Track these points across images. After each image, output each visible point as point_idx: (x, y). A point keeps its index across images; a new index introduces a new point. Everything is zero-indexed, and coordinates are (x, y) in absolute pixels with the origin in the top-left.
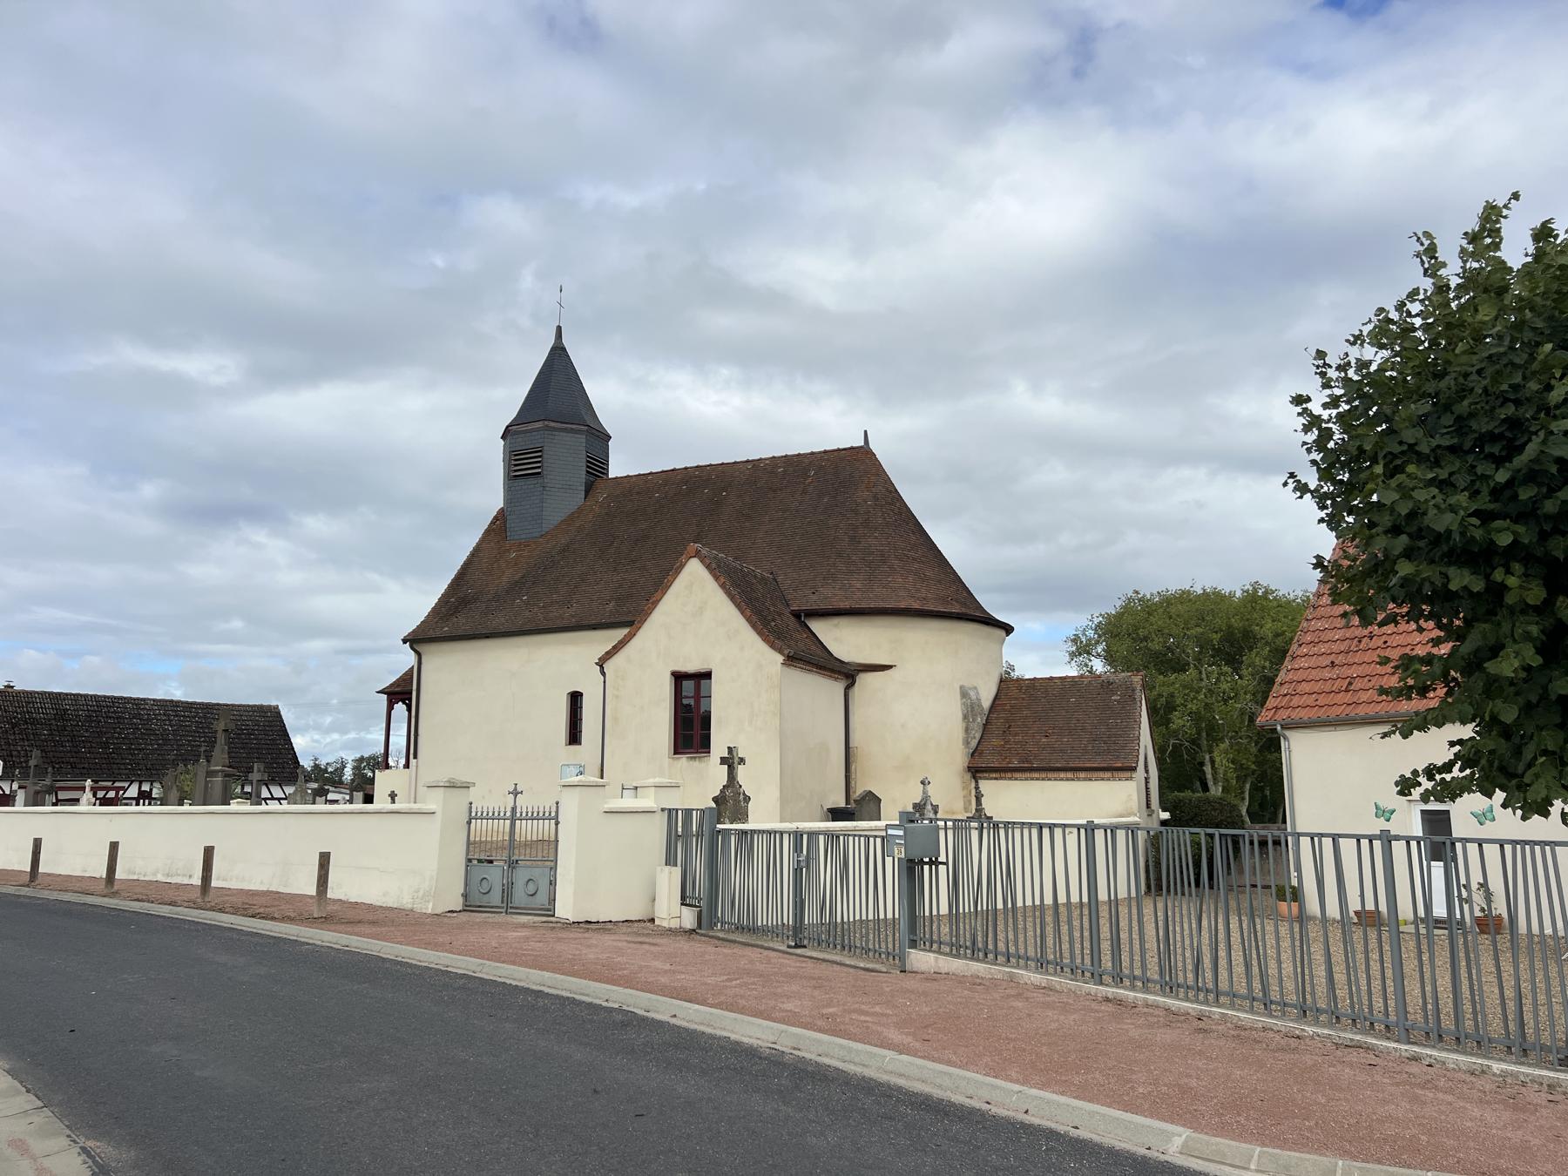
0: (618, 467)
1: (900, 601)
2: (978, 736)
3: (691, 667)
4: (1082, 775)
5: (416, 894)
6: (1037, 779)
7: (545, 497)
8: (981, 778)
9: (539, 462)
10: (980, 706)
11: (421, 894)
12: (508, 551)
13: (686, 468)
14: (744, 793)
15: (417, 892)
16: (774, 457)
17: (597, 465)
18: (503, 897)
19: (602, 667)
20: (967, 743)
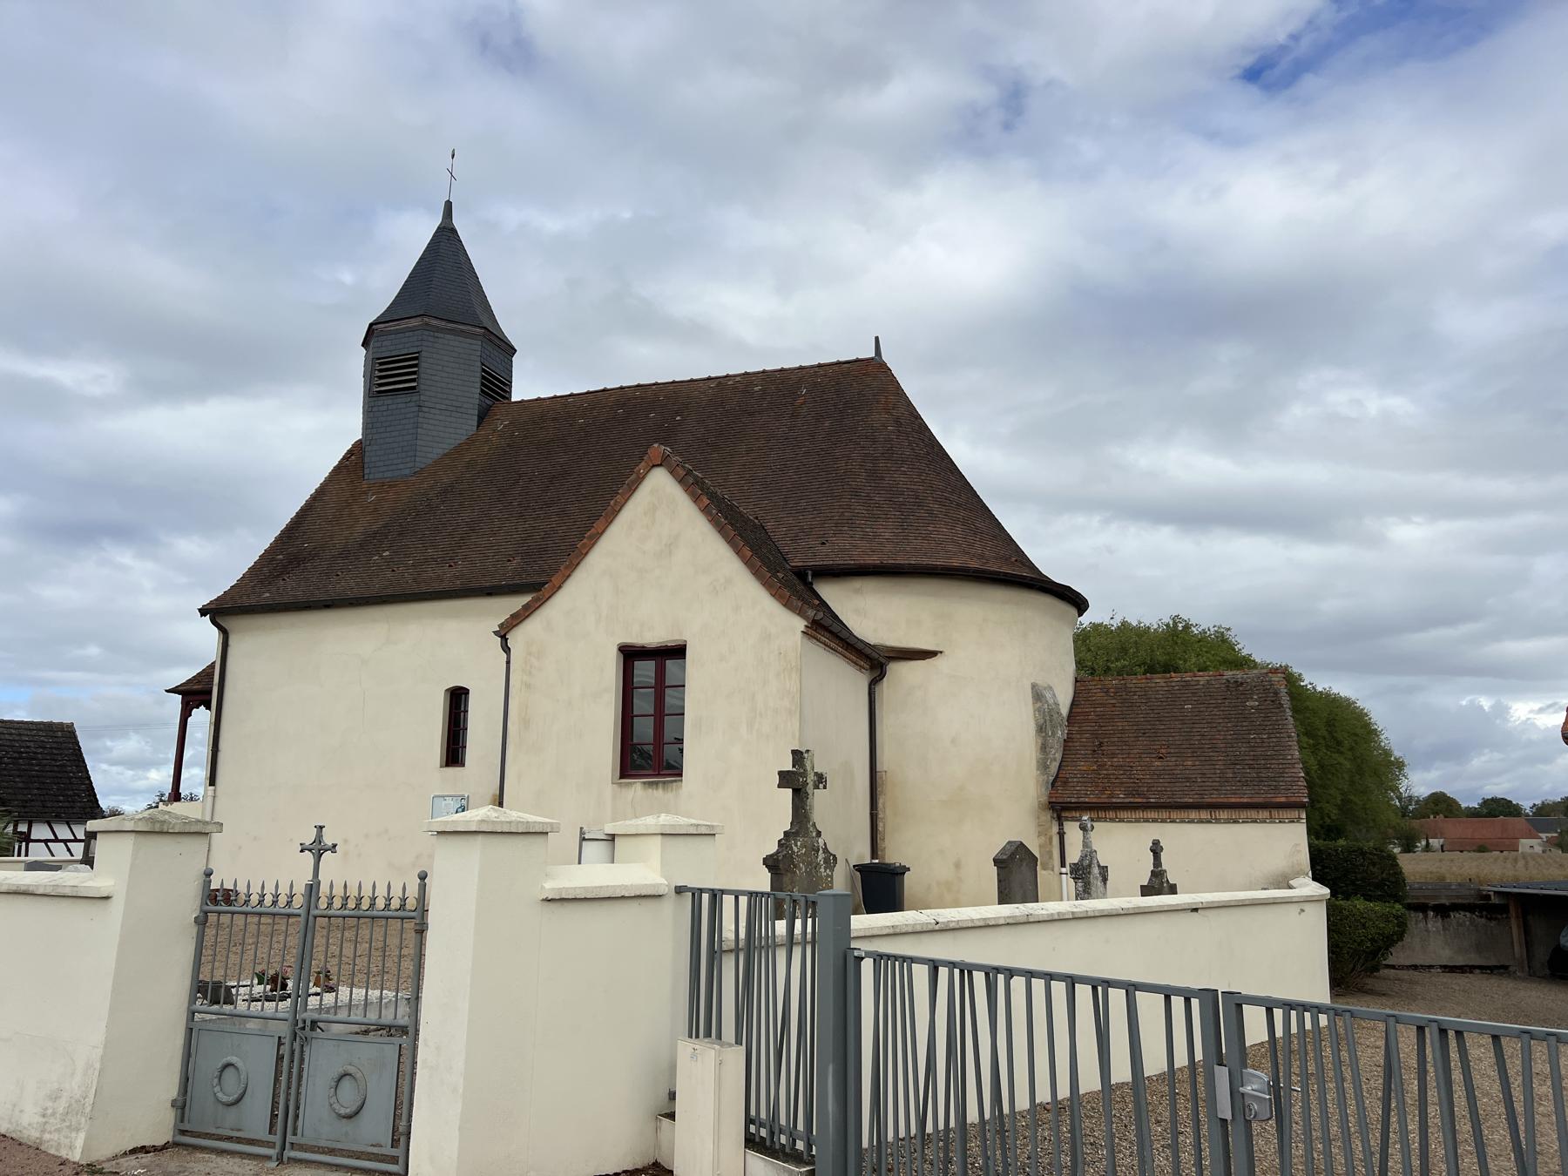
0: (527, 386)
1: (951, 558)
2: (1059, 756)
3: (652, 637)
4: (1224, 814)
5: (49, 1104)
6: (1155, 821)
7: (421, 420)
8: (1067, 819)
9: (414, 373)
10: (1059, 713)
11: (61, 1106)
12: (365, 493)
13: (622, 388)
14: (826, 850)
15: (55, 1097)
16: (746, 373)
17: (496, 385)
18: (274, 1116)
19: (504, 638)
20: (1043, 766)
